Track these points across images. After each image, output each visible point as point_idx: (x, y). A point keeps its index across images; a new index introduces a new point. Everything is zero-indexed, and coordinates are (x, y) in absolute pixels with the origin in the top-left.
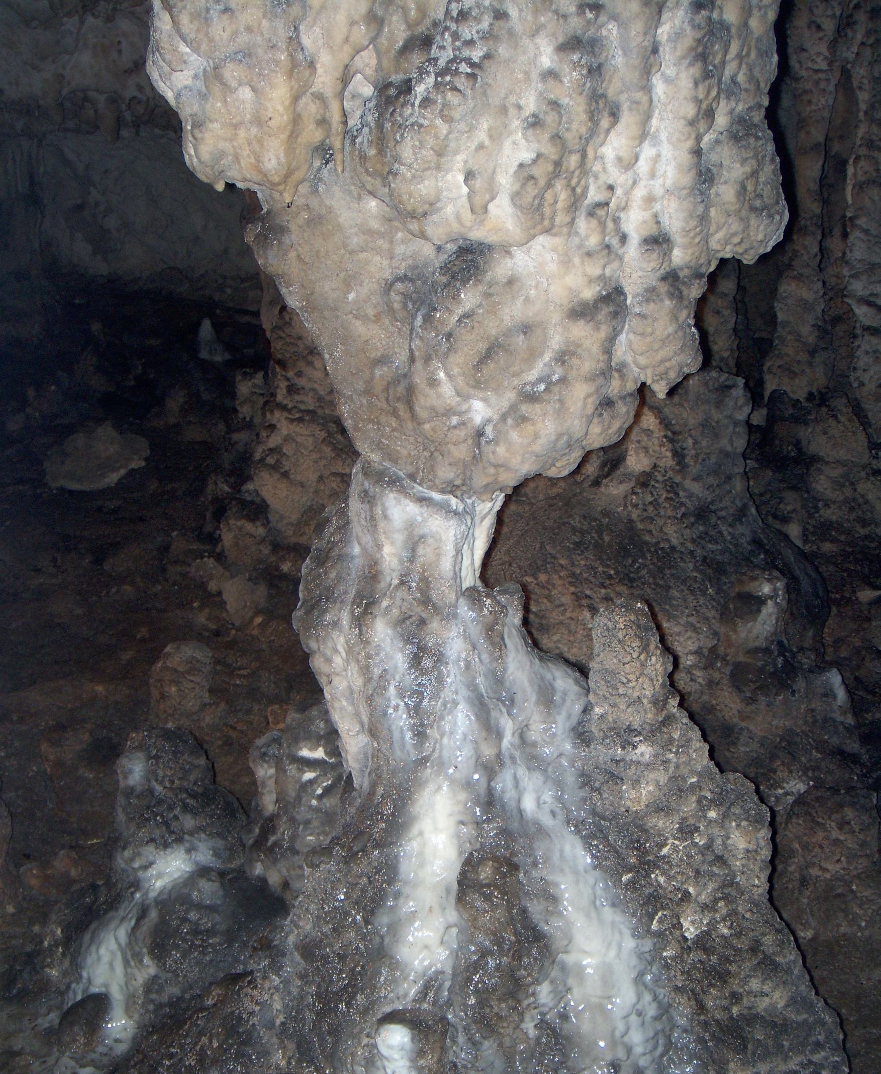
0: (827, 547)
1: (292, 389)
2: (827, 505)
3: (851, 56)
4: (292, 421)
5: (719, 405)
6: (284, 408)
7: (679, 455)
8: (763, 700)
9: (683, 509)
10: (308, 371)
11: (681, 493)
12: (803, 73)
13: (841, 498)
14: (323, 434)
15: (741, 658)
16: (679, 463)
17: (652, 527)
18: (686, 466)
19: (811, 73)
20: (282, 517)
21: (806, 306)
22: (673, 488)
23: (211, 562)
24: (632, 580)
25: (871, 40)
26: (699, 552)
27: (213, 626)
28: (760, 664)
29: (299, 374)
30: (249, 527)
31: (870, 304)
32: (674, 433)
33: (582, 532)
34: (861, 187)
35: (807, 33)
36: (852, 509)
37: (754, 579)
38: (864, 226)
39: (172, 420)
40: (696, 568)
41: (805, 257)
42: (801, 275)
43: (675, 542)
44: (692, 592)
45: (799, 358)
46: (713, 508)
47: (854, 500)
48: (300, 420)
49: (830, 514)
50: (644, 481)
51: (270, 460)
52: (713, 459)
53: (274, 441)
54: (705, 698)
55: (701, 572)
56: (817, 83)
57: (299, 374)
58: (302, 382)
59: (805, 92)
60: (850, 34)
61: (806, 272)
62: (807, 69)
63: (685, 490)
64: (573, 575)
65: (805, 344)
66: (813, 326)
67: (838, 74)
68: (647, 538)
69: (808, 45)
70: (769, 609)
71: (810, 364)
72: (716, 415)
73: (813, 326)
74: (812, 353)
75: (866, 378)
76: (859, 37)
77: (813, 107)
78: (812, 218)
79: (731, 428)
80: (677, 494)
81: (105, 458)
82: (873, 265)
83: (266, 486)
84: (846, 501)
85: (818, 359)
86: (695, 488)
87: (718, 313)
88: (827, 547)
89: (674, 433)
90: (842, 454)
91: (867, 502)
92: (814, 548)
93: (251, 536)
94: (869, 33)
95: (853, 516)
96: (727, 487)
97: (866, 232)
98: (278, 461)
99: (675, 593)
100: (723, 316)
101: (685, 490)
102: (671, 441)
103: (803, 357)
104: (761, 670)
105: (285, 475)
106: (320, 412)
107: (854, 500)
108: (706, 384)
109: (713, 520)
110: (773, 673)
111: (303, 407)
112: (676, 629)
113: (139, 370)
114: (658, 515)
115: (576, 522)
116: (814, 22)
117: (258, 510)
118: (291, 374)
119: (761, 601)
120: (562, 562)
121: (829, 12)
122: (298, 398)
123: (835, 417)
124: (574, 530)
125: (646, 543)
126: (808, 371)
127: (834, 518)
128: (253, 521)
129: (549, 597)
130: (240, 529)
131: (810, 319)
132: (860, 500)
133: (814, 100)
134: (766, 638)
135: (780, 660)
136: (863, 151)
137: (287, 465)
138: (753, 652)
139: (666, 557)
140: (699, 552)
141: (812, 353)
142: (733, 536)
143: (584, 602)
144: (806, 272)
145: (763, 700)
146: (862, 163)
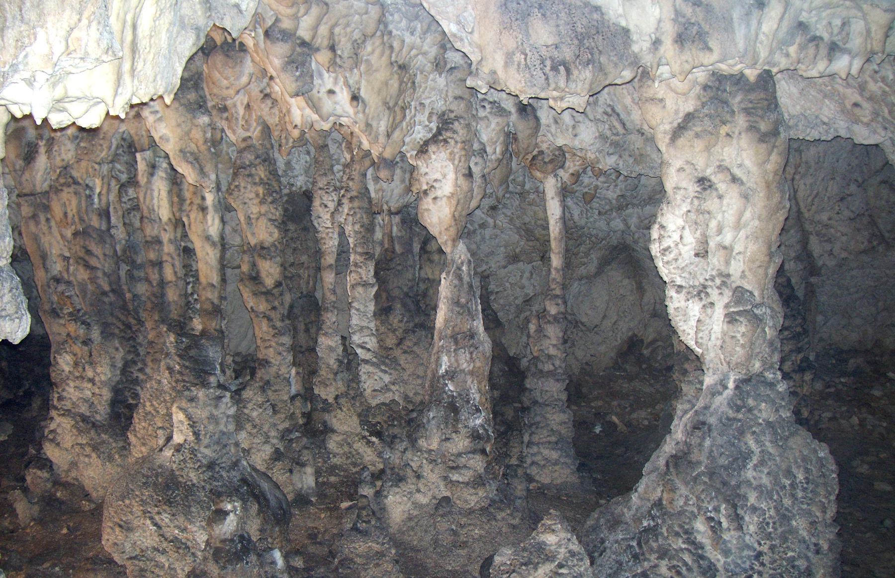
0: (333, 479)
1: (60, 399)
2: (335, 456)
3: (342, 220)
4: (59, 415)
5: (216, 406)
6: (56, 408)
7: (196, 434)
8: (230, 567)
9: (199, 464)
10: (67, 388)
11: (199, 455)
12: (320, 229)
13: (342, 452)
14: (73, 422)
15: (218, 545)
16: (196, 439)
17: (183, 474)
18: (201, 440)
20: (59, 467)
21: (331, 349)
22: (193, 452)
23: (17, 492)
24: (171, 503)
26: (208, 487)
27: (11, 528)
28: (227, 548)
29: (64, 390)
30: (39, 473)
31: (363, 348)
32: (194, 422)
33: (148, 477)
35: (320, 209)
36: (348, 458)
37: (222, 501)
39: (35, 414)
40: (206, 496)
41: (328, 324)
43: (195, 481)
44: (202, 509)
46: (218, 462)
47: (350, 453)
48: (63, 415)
49: (336, 461)
50: (178, 448)
51: (51, 437)
52: (217, 436)
53: (53, 426)
54: (202, 566)
55: (208, 497)
56: (327, 234)
57: (64, 390)
58: (65, 394)
59: (322, 238)
60: (341, 209)
61: (330, 331)
63: (200, 453)
64: (142, 500)
67: (337, 230)
68: (181, 479)
69: (322, 215)
70: (231, 517)
71: (335, 380)
72: (215, 413)
74: (336, 374)
75: (366, 386)
76: (346, 211)
79: (225, 419)
80: (196, 455)
83: (50, 451)
84: (345, 453)
85: (339, 377)
86: (207, 452)
87: (280, 354)
88: (333, 479)
89: (194, 422)
90: (345, 428)
91: (358, 454)
92: (325, 480)
93: (40, 478)
94: (350, 209)
95: (349, 461)
96: (224, 451)
97: (358, 310)
98: (54, 437)
99: (193, 509)
101: (200, 453)
102: (192, 426)
103: (331, 376)
104: (229, 551)
105: (58, 444)
106: (73, 410)
107: (350, 453)
108: (207, 396)
109: (217, 469)
110: (235, 553)
111: (65, 408)
112: (195, 529)
113: (27, 387)
114: (186, 467)
115: (145, 471)
117: (46, 464)
118: (60, 390)
119: (226, 513)
120: (137, 493)
121: (331, 199)
122: (63, 403)
123: (341, 409)
124: (144, 475)
125: (180, 482)
127: (338, 463)
128: (41, 470)
129: (131, 512)
130: (35, 473)
131: (334, 356)
132: (354, 453)
134: (231, 534)
135: (239, 545)
136: (353, 268)
137: (59, 439)
138: (223, 541)
139: (190, 490)
140: (208, 487)
141: (336, 374)
142: (229, 477)
143: (147, 515)
144: (330, 331)
145: (230, 567)
146: (353, 274)
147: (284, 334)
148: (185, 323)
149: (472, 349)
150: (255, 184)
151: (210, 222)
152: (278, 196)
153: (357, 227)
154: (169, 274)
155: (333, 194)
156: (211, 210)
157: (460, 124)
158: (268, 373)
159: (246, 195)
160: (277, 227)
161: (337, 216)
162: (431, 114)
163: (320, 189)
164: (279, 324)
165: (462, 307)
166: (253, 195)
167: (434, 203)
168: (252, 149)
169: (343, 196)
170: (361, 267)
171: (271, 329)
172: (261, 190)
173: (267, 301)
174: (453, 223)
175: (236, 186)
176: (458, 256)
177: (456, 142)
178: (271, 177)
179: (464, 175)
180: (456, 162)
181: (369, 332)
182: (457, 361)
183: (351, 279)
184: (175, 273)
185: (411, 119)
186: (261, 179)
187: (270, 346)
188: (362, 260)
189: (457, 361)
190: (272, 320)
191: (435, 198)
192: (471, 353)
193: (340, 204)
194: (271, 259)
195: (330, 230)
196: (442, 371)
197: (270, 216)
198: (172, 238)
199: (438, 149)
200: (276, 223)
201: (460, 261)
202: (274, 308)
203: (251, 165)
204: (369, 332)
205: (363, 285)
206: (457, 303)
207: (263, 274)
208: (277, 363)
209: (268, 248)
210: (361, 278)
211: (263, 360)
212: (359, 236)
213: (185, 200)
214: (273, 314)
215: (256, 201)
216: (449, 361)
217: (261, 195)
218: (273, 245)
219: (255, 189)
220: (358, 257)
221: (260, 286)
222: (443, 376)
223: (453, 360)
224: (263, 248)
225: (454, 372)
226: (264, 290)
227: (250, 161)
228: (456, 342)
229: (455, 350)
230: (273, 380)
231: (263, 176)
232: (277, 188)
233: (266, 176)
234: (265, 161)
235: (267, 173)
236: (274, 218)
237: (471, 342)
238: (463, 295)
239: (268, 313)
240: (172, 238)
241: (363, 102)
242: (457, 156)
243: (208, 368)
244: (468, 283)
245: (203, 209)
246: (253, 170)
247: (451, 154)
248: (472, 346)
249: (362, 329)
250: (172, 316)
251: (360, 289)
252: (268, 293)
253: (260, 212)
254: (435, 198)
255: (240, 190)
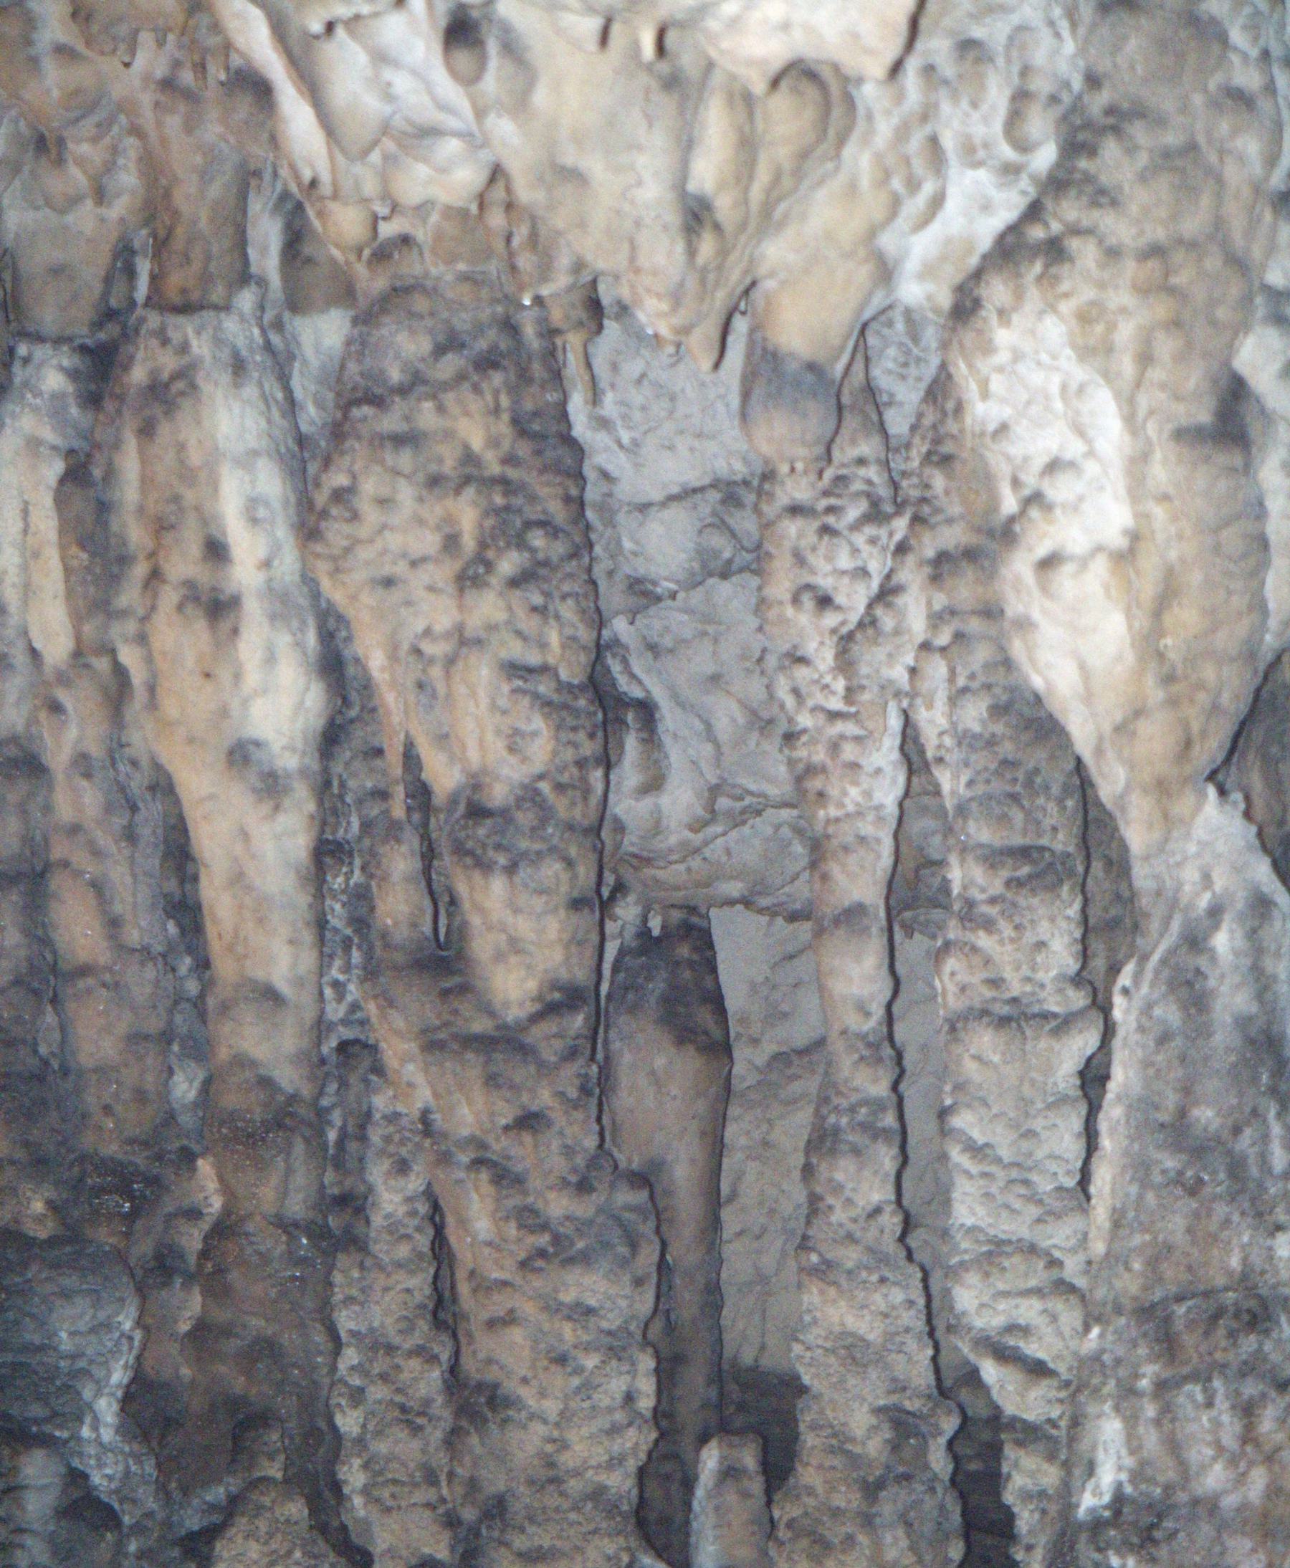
12: (805, 720)
19: (821, 718)
21: (853, 1352)
25: (943, 638)
34: (953, 1029)
38: (978, 1136)
41: (839, 1216)
42: (829, 1264)
45: (839, 1501)
56: (835, 747)
60: (887, 622)
61: (851, 1256)
62: (817, 709)
65: (854, 1460)
66: (878, 1411)
71: (868, 1521)
73: (878, 1411)
74: (872, 1490)
76: (917, 624)
77: (833, 812)
78: (853, 1110)
81: (1135, 1540)
82: (999, 1243)
85: (887, 1507)
87: (562, 1360)
94: (936, 620)
97: (976, 1151)
100: (579, 1371)
116: (808, 587)
121: (845, 562)
126: (862, 1538)
133: (834, 792)
141: (872, 1490)
147: (585, 1259)
148: (154, 1181)
149: (1250, 1389)
150: (434, 481)
151: (253, 677)
152: (559, 548)
153: (974, 714)
154: (77, 930)
155: (860, 539)
156: (253, 609)
157: (1131, 151)
158: (501, 1457)
159: (394, 541)
160: (546, 704)
161: (871, 659)
162: (1021, 97)
163: (795, 510)
164: (558, 1206)
165: (1199, 1152)
166: (429, 542)
167: (1045, 589)
168: (420, 304)
169: (902, 549)
170: (988, 925)
171: (512, 1230)
172: (467, 513)
173: (492, 1081)
174: (1156, 694)
175: (339, 496)
176: (1190, 875)
177: (1113, 254)
178: (524, 449)
179: (1186, 435)
180: (1127, 366)
181: (1039, 1276)
182: (1174, 1446)
183: (954, 981)
184: (114, 924)
185: (902, 133)
186: (469, 458)
187: (510, 1319)
188: (997, 887)
189: (1174, 1446)
190: (518, 1181)
191: (1049, 563)
192: (1248, 1411)
193: (887, 593)
194: (511, 869)
195: (850, 728)
196: (1090, 1501)
197: (515, 650)
198: (96, 750)
199: (1019, 295)
200: (544, 687)
201: (1204, 901)
202: (529, 1121)
203: (415, 383)
204: (1039, 1276)
205: (1004, 1021)
206: (1177, 1131)
207: (482, 946)
208: (551, 1407)
209: (504, 814)
210: (995, 983)
211: (480, 1386)
212: (981, 759)
213: (124, 560)
214: (520, 1152)
215: (443, 573)
216: (1133, 1443)
217: (469, 543)
218: (529, 795)
219: (435, 510)
220: (978, 873)
221: (466, 1008)
222: (1097, 1526)
223: (1151, 1440)
224: (477, 812)
225: (1160, 1510)
226: (481, 1025)
227: (406, 366)
228: (1168, 1345)
229: (1162, 1386)
230: (524, 1498)
231: (477, 443)
232: (557, 511)
233: (493, 442)
234: (487, 363)
235: (503, 427)
236: (534, 659)
237: (1249, 1343)
238: (1211, 1085)
239: (500, 1145)
240: (96, 750)
241: (512, 49)
242: (1126, 332)
243: (36, 1410)
244: (1242, 1022)
245: (218, 608)
246: (427, 416)
247: (1085, 318)
248: (1248, 1369)
249: (996, 1251)
250: (88, 1141)
251: (984, 1040)
252: (504, 1043)
253: (460, 628)
254: (1049, 563)
255: (355, 516)
